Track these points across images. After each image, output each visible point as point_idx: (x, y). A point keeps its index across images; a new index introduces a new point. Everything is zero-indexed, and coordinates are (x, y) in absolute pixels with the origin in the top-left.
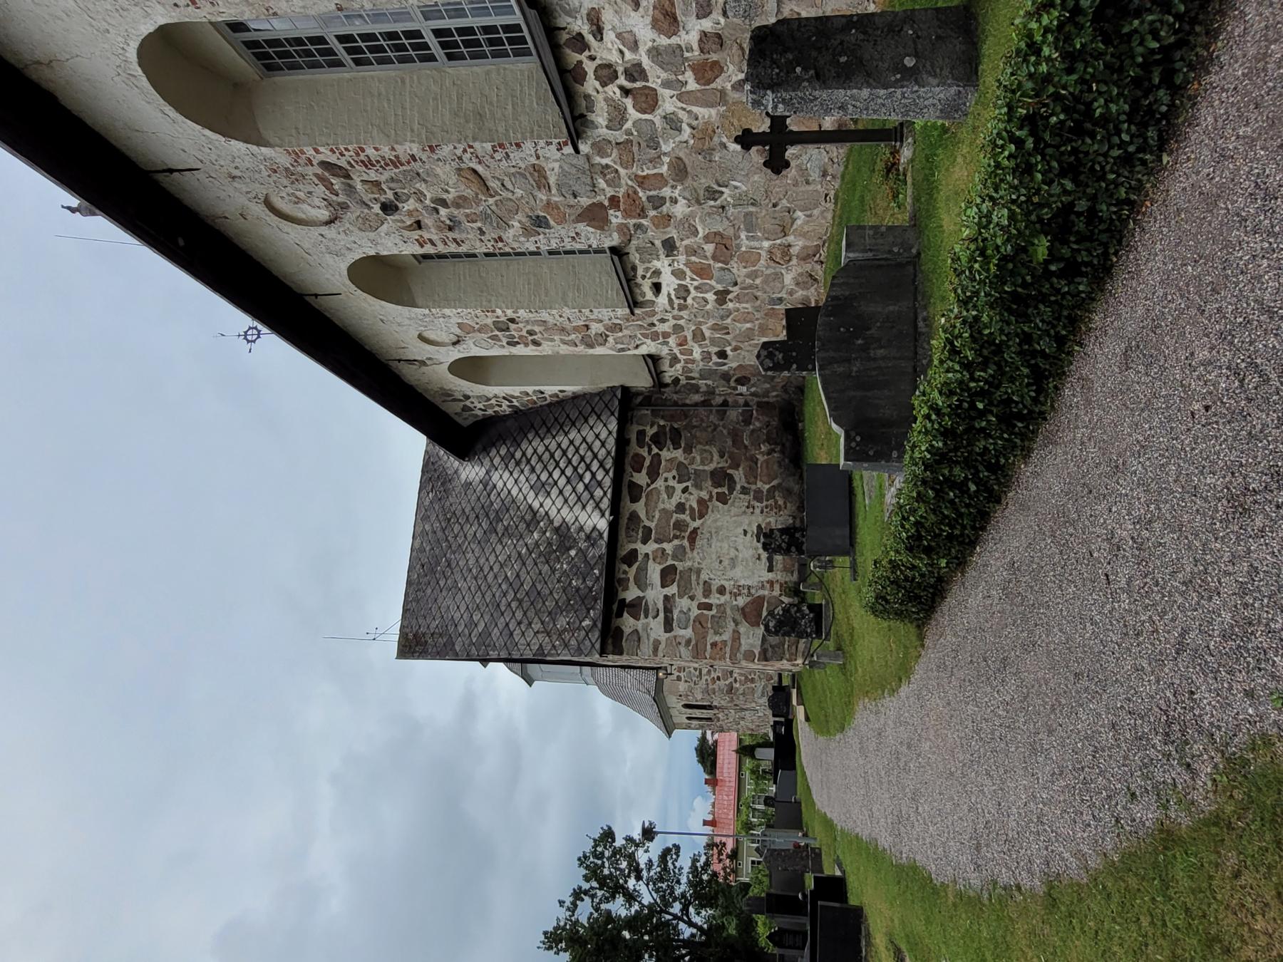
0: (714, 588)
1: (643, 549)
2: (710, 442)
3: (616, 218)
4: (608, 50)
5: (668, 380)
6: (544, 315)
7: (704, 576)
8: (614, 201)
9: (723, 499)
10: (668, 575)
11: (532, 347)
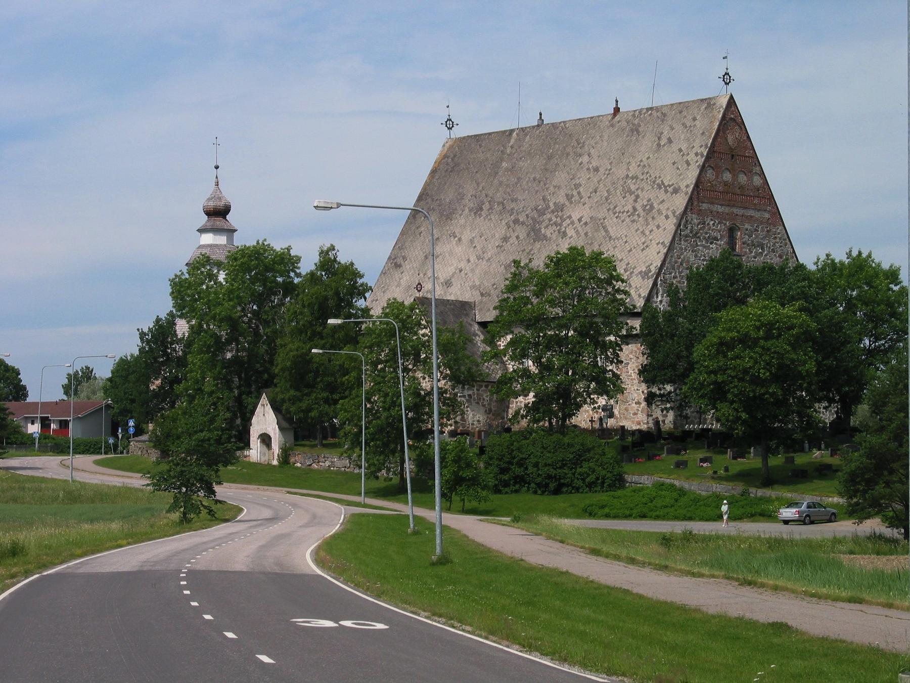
9: (486, 411)
10: (470, 396)
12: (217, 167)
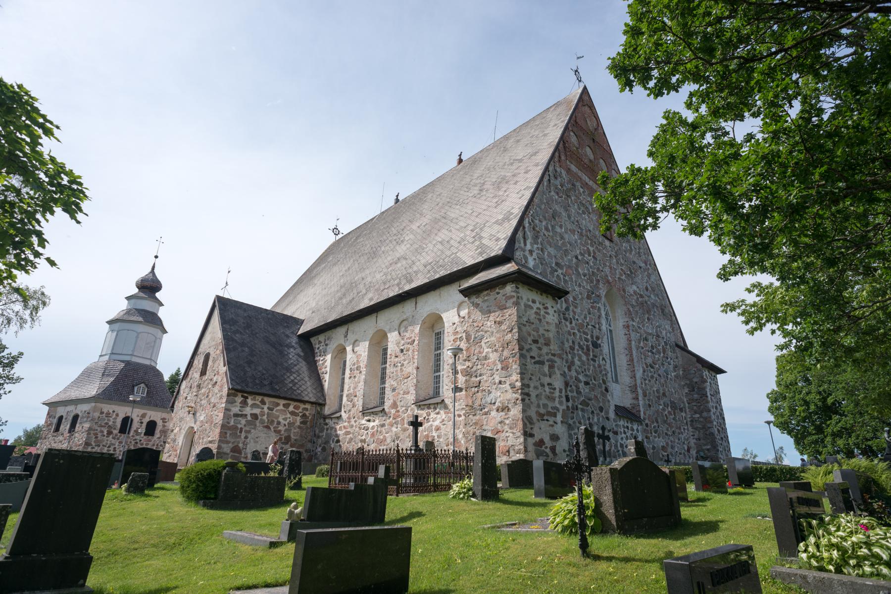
0: (247, 434)
1: (266, 407)
2: (301, 436)
3: (393, 411)
4: (433, 415)
5: (327, 421)
6: (362, 383)
7: (252, 431)
8: (398, 411)
10: (255, 416)
11: (349, 376)
12: (156, 257)
